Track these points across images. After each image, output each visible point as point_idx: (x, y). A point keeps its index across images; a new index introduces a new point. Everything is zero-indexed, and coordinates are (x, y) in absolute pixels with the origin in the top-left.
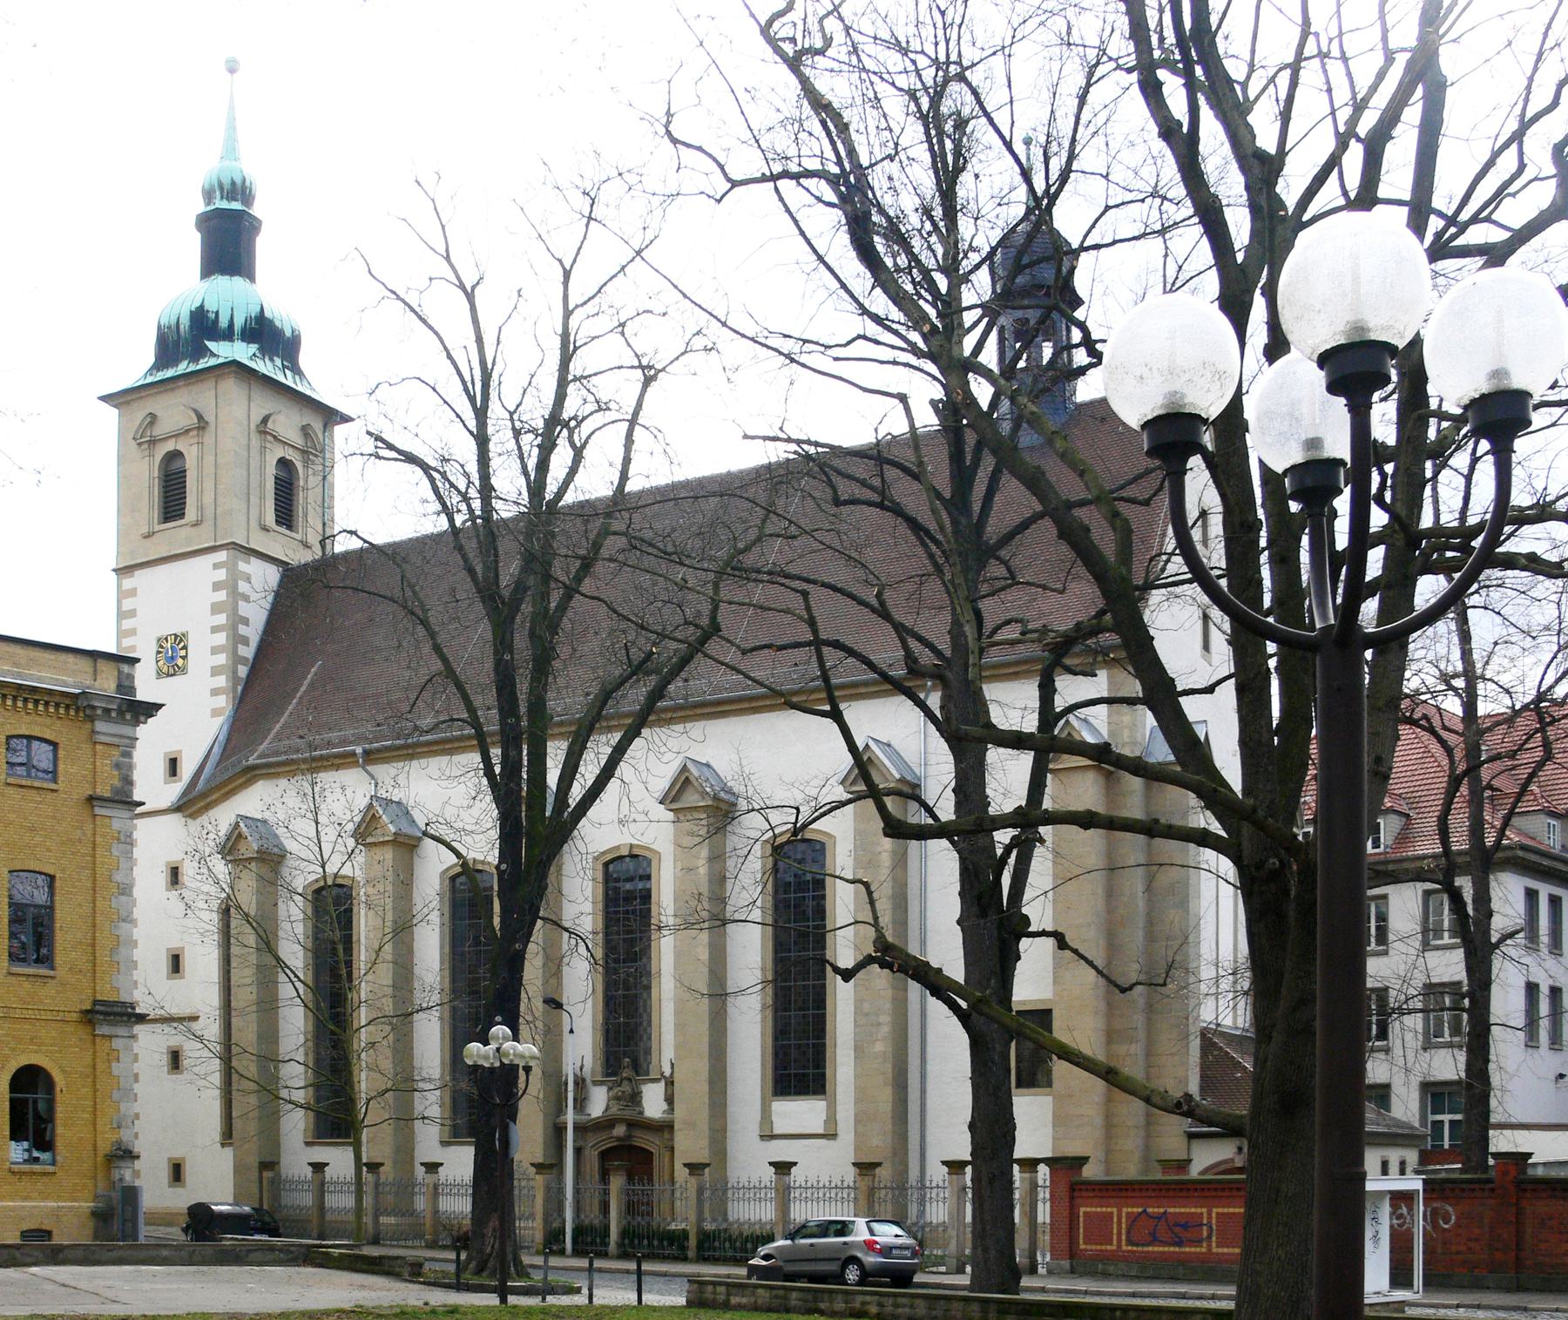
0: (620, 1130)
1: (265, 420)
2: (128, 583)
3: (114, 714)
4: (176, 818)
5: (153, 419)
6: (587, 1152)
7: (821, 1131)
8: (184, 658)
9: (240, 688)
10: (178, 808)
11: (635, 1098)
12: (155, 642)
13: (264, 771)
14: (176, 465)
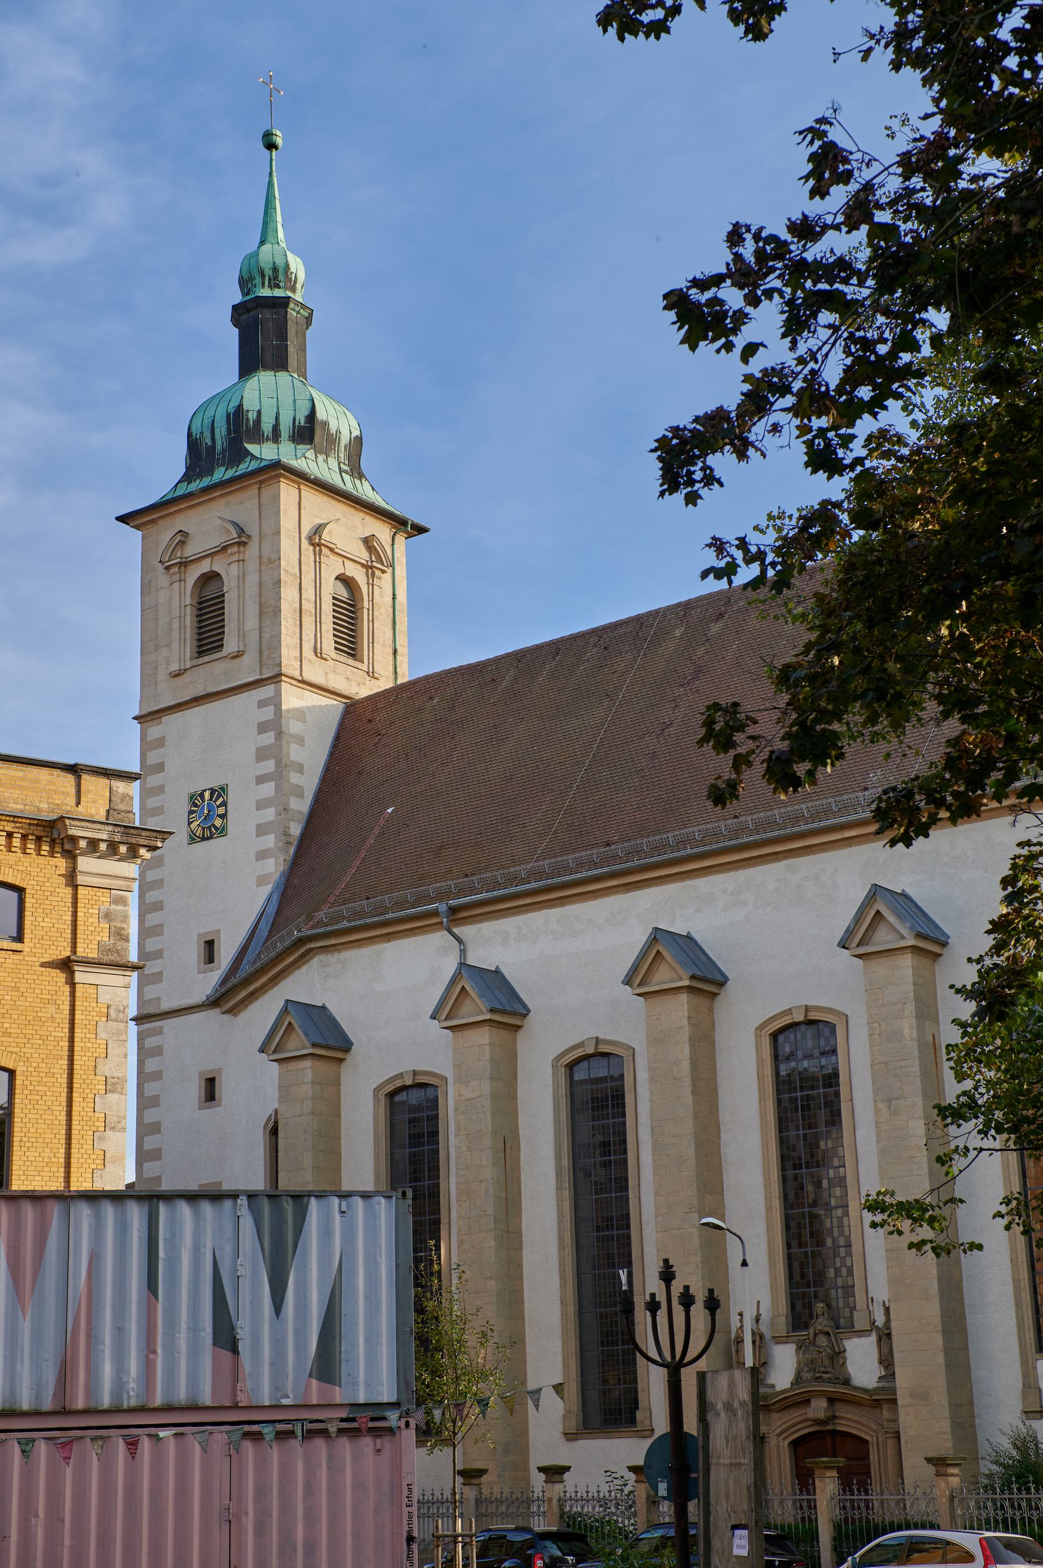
1: (319, 529)
2: (155, 731)
3: (103, 846)
4: (214, 1013)
5: (183, 537)
6: (772, 1442)
8: (223, 816)
9: (292, 850)
10: (214, 1002)
11: (838, 1355)
13: (320, 944)
14: (210, 591)
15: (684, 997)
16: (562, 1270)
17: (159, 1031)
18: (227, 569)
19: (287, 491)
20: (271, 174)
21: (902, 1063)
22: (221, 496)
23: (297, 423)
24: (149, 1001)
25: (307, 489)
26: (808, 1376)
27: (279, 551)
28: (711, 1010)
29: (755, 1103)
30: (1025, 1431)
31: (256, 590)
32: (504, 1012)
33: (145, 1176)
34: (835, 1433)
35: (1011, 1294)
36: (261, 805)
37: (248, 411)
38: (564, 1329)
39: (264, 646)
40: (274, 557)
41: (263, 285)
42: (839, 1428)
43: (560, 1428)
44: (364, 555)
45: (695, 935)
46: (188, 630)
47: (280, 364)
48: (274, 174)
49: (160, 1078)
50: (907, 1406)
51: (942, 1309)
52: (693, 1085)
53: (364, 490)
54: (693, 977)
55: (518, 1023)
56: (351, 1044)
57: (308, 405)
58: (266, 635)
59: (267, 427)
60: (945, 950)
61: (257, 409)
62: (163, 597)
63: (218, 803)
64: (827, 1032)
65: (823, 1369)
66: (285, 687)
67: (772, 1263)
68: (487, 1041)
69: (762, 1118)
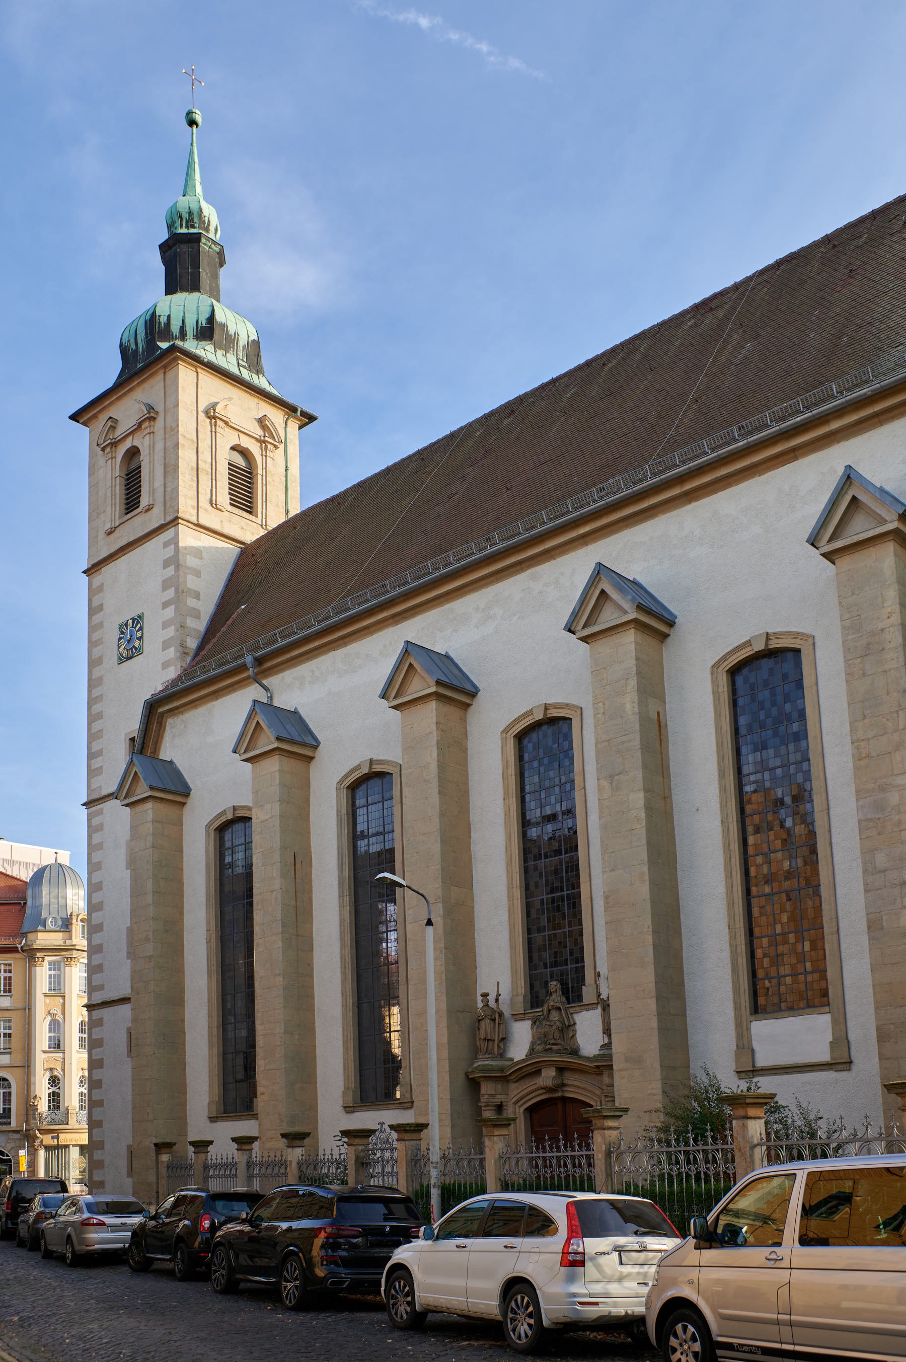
0: (548, 1076)
5: (113, 423)
7: (826, 1057)
8: (140, 639)
11: (568, 1028)
12: (117, 629)
15: (433, 704)
16: (343, 967)
17: (101, 812)
18: (141, 441)
19: (185, 373)
20: (192, 144)
21: (624, 738)
22: (139, 384)
23: (200, 324)
24: (95, 789)
25: (203, 372)
26: (539, 1048)
27: (177, 420)
28: (464, 720)
29: (500, 802)
30: (706, 1080)
31: (162, 454)
32: (292, 742)
33: (93, 923)
34: (564, 1099)
35: (728, 960)
36: (165, 625)
37: (160, 316)
38: (344, 1017)
39: (167, 498)
40: (174, 425)
41: (182, 227)
42: (567, 1095)
43: (340, 1103)
44: (259, 432)
45: (452, 655)
46: (118, 496)
47: (194, 286)
48: (195, 144)
49: (101, 848)
50: (621, 1070)
51: (657, 974)
52: (440, 786)
53: (261, 382)
54: (439, 683)
55: (310, 754)
56: (190, 790)
57: (209, 310)
58: (168, 489)
59: (175, 328)
60: (672, 630)
61: (167, 314)
62: (101, 474)
63: (137, 629)
64: (565, 729)
65: (552, 1041)
66: (182, 528)
67: (512, 948)
68: (277, 768)
69: (505, 815)
